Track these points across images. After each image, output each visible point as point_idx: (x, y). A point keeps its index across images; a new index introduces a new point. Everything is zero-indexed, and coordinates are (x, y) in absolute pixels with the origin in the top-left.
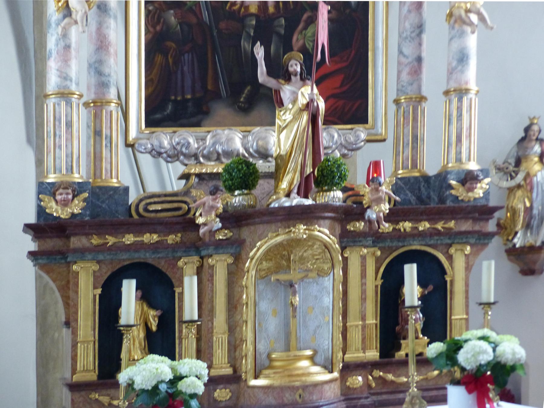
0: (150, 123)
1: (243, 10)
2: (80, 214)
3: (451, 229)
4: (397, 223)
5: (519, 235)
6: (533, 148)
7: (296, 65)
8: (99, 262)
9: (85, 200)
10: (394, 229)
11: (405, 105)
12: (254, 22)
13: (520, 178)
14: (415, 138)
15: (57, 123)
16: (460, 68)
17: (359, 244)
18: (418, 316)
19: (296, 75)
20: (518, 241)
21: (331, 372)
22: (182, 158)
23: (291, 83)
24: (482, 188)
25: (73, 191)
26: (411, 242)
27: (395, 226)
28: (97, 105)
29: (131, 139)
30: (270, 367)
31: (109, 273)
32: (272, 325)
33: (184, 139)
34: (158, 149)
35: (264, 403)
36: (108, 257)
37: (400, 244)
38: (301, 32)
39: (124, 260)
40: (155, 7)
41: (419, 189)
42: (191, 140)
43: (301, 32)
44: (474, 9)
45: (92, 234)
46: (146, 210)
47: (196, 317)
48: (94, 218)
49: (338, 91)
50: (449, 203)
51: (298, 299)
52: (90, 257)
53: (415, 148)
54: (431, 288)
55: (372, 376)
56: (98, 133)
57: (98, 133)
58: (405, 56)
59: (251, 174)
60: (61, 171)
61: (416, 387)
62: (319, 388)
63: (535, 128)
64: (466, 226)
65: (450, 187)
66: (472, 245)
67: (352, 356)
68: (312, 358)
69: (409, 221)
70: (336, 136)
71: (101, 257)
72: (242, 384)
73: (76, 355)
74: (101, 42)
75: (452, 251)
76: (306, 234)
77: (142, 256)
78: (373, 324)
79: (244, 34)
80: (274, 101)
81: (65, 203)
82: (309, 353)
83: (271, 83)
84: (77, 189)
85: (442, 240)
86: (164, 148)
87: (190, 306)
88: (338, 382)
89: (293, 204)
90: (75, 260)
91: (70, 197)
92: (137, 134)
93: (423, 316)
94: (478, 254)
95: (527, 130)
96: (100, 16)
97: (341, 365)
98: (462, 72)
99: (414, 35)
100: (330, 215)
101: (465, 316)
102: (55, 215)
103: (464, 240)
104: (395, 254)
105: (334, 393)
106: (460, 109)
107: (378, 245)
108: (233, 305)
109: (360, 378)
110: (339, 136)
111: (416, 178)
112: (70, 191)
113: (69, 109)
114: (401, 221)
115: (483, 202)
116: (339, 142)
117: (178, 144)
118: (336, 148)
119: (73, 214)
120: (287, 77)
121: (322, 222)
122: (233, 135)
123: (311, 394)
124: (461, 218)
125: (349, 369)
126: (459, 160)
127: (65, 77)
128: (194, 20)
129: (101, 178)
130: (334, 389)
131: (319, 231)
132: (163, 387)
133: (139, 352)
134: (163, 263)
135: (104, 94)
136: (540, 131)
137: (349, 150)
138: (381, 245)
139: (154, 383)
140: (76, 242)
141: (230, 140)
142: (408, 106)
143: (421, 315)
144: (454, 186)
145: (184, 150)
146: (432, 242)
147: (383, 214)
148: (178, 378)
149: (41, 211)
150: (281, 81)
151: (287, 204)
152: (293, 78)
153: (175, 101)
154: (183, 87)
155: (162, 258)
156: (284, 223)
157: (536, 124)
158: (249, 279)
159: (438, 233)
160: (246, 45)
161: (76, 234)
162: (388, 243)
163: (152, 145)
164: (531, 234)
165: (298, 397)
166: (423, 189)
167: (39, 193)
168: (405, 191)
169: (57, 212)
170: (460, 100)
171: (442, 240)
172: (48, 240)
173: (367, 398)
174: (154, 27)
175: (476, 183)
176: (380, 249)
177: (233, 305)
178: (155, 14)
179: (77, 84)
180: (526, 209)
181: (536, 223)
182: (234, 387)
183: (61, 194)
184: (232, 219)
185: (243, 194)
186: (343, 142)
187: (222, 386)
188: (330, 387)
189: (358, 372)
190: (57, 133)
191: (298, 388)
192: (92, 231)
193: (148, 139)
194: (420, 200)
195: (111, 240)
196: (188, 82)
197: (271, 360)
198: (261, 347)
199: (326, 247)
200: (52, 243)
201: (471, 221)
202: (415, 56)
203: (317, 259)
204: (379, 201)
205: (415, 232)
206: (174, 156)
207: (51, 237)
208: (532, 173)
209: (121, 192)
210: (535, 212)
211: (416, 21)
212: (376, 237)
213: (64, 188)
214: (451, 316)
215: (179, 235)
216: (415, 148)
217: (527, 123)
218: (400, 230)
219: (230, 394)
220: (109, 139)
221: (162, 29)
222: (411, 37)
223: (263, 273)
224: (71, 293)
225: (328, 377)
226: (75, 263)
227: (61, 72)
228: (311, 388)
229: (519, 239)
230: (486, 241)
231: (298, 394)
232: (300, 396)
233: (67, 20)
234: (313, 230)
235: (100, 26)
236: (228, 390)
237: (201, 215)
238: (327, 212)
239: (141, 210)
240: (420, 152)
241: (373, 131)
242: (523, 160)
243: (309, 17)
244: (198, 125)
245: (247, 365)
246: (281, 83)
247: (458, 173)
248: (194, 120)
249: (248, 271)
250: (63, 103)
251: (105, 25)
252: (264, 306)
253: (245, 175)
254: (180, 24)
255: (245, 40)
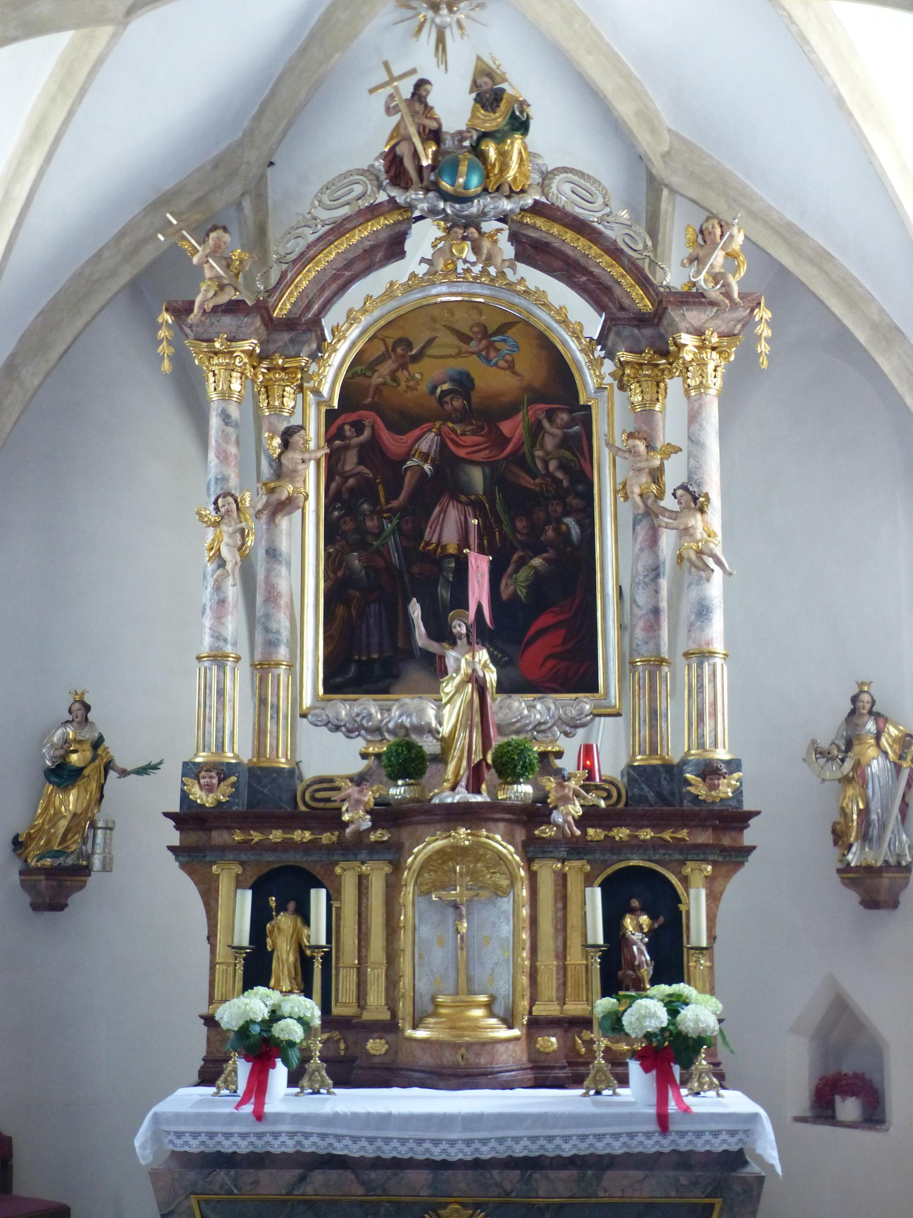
0: (330, 688)
1: (439, 550)
2: (227, 801)
3: (683, 840)
4: (610, 830)
5: (854, 849)
6: (865, 725)
7: (460, 626)
8: (242, 863)
9: (233, 785)
10: (606, 836)
11: (641, 670)
12: (453, 565)
13: (848, 764)
14: (653, 713)
15: (208, 691)
16: (698, 623)
17: (550, 855)
18: (643, 959)
19: (460, 638)
20: (853, 858)
21: (510, 1027)
22: (363, 732)
23: (456, 648)
24: (729, 785)
25: (218, 774)
26: (629, 856)
27: (606, 833)
28: (263, 668)
29: (304, 707)
30: (434, 1014)
31: (255, 878)
32: (438, 957)
33: (365, 709)
34: (336, 722)
35: (421, 1062)
36: (252, 858)
37: (615, 858)
38: (511, 576)
39: (269, 862)
40: (336, 549)
41: (659, 783)
42: (373, 711)
43: (511, 576)
44: (706, 551)
45: (234, 828)
46: (313, 798)
47: (323, 942)
48: (251, 808)
49: (557, 650)
50: (687, 805)
51: (465, 925)
52: (231, 857)
53: (653, 727)
54: (662, 919)
55: (580, 1038)
56: (262, 701)
57: (262, 701)
58: (638, 606)
59: (413, 760)
60: (210, 749)
61: (603, 1058)
62: (488, 1048)
63: (865, 697)
64: (704, 837)
65: (687, 783)
66: (714, 863)
67: (547, 1008)
68: (489, 1006)
69: (626, 826)
70: (552, 707)
71: (243, 858)
72: (400, 1034)
73: (214, 980)
74: (269, 592)
75: (687, 870)
76: (469, 840)
77: (292, 859)
78: (582, 964)
79: (441, 578)
80: (436, 668)
81: (209, 789)
82: (483, 998)
83: (434, 647)
84: (223, 771)
85: (670, 854)
86: (341, 721)
87: (698, 931)
88: (523, 1043)
89: (455, 801)
90: (214, 859)
91: (215, 781)
92: (313, 702)
93: (651, 960)
94: (730, 877)
95: (855, 699)
96: (268, 563)
97: (526, 1018)
98: (702, 630)
99: (647, 580)
100: (507, 816)
101: (584, 962)
102: (199, 801)
103: (702, 857)
104: (610, 871)
105: (514, 1058)
106: (700, 677)
107: (585, 857)
108: (392, 928)
109: (553, 1040)
110: (557, 708)
111: (654, 767)
112: (214, 774)
113: (222, 674)
114: (615, 826)
115: (733, 803)
116: (557, 717)
117: (358, 715)
118: (554, 724)
119: (219, 803)
120: (452, 640)
121: (491, 825)
122: (424, 705)
123: (478, 1055)
124: (696, 826)
125: (536, 1025)
126: (701, 746)
127: (218, 637)
128: (381, 563)
129: (265, 756)
130: (515, 1052)
131: (487, 837)
132: (255, 1030)
133: (288, 982)
134: (318, 867)
135: (270, 654)
136: (873, 702)
137: (571, 727)
138: (590, 857)
139: (241, 1022)
140: (219, 837)
141: (421, 712)
142: (644, 671)
143: (648, 958)
144: (693, 782)
145: (364, 722)
146: (657, 857)
147: (573, 818)
148: (275, 1016)
149: (185, 797)
150: (445, 644)
151: (449, 800)
152: (459, 642)
153: (359, 662)
154: (368, 645)
155: (317, 862)
156: (444, 824)
157: (867, 692)
158: (408, 894)
159: (665, 844)
160: (444, 594)
161: (217, 828)
162: (598, 856)
163: (327, 716)
164: (870, 848)
165: (460, 1058)
166: (664, 783)
167: (184, 775)
168: (639, 784)
169: (202, 800)
170: (700, 666)
171: (670, 854)
172: (192, 834)
173: (563, 1068)
174: (335, 572)
175: (719, 779)
176: (589, 862)
177: (392, 928)
178: (336, 557)
179: (235, 644)
180: (860, 812)
181: (875, 832)
182: (391, 1037)
183: (204, 778)
184: (386, 814)
185: (409, 785)
186: (563, 716)
187: (376, 1035)
188: (507, 1048)
189: (551, 1031)
190: (208, 703)
191: (459, 1046)
192: (234, 825)
193: (323, 709)
194: (660, 796)
195: (256, 836)
196: (375, 640)
197: (437, 1006)
198: (423, 985)
199: (501, 859)
200: (195, 837)
201: (710, 831)
202: (650, 607)
203: (494, 873)
204: (566, 800)
205: (634, 842)
206: (351, 731)
207: (194, 830)
208: (864, 761)
209: (286, 775)
210: (874, 817)
211: (650, 562)
212: (576, 848)
213: (206, 771)
214: (688, 962)
215: (337, 833)
216: (653, 727)
217: (856, 691)
218: (614, 838)
219: (387, 1046)
220: (275, 708)
221: (344, 574)
222: (644, 583)
223: (426, 887)
224: (212, 902)
225: (504, 1033)
226: (215, 863)
227: (214, 631)
228: (477, 1047)
229: (855, 854)
230: (740, 859)
231: (460, 1052)
232: (463, 1056)
233: (219, 572)
234: (480, 837)
235: (597, 292)
236: (383, 1041)
237: (347, 810)
238: (496, 813)
239: (307, 798)
240: (661, 732)
241: (604, 702)
242: (855, 742)
243: (520, 557)
244: (386, 691)
245: (404, 1008)
246: (445, 648)
247: (697, 763)
248: (381, 685)
249: (406, 885)
250: (215, 668)
251: (273, 573)
252: (425, 931)
253: (405, 760)
254: (365, 568)
255: (442, 587)
